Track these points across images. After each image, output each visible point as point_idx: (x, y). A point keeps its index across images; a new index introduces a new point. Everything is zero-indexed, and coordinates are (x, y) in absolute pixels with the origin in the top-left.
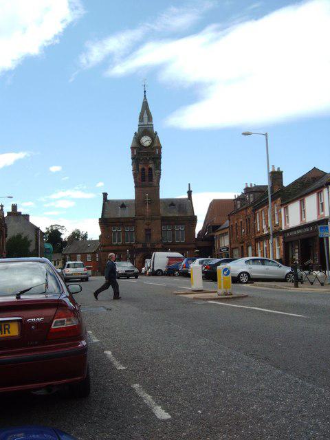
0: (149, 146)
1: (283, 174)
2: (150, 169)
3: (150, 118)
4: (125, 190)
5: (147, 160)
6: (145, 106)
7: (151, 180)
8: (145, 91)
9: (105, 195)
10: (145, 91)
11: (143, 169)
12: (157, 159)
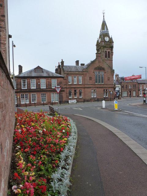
0: (107, 42)
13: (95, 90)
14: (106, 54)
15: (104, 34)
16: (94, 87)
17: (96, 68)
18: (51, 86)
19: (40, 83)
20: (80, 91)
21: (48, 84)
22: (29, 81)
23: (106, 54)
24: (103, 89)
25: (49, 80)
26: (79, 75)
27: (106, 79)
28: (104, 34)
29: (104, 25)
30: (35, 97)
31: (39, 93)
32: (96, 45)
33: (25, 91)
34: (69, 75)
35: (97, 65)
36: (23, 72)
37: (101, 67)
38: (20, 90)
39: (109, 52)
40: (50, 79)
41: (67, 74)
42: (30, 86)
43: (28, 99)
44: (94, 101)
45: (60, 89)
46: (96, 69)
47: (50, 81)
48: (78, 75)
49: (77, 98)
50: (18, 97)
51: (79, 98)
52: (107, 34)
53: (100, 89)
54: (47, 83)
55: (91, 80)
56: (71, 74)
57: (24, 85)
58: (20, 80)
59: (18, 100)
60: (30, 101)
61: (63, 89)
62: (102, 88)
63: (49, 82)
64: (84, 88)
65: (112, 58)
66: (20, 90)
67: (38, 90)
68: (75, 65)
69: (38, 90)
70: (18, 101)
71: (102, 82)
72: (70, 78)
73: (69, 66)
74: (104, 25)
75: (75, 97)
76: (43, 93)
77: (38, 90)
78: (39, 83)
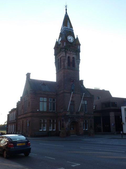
1: (84, 81)
2: (73, 58)
4: (48, 73)
5: (68, 49)
6: (67, 20)
7: (74, 66)
8: (66, 10)
9: (28, 75)
10: (66, 10)
11: (69, 57)
12: (78, 51)
29: (67, 20)
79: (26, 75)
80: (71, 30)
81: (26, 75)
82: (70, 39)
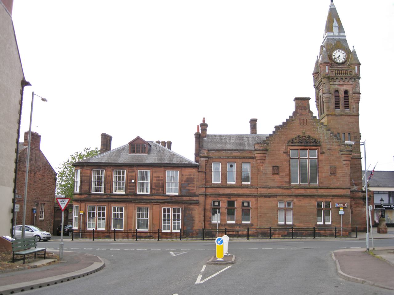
0: (343, 63)
1: (257, 122)
3: (341, 29)
9: (204, 126)
13: (289, 204)
14: (337, 98)
15: (335, 42)
16: (286, 193)
17: (293, 140)
18: (164, 189)
19: (136, 180)
20: (246, 204)
21: (155, 183)
22: (109, 173)
23: (337, 98)
24: (314, 202)
25: (159, 173)
26: (244, 160)
27: (326, 169)
28: (335, 42)
29: (333, 15)
30: (122, 216)
31: (131, 206)
32: (313, 74)
33: (98, 200)
34: (214, 160)
35: (296, 132)
36: (112, 149)
37: (309, 137)
38: (86, 196)
39: (346, 92)
40: (162, 169)
41: (209, 157)
42: (111, 186)
43: (103, 219)
44: (285, 236)
45: (67, 200)
46: (292, 143)
47: (161, 175)
48: (241, 160)
49: (236, 225)
50: (82, 213)
51: (226, 225)
52: (339, 41)
53: (305, 202)
54: (154, 181)
55: (278, 173)
56: (219, 157)
57: (282, 170)
58: (89, 172)
59: (80, 219)
60: (108, 225)
61: (195, 198)
62: (311, 196)
63: (159, 177)
64: (256, 196)
65: (358, 109)
66: (86, 196)
67: (132, 198)
68: (250, 134)
69: (130, 197)
70: (80, 222)
71: (313, 180)
72: (216, 168)
73: (220, 136)
74: (333, 15)
75: (228, 222)
76: (141, 206)
77: (130, 197)
78: (133, 181)
79: (276, 127)
80: (341, 38)
81: (276, 127)
82: (339, 56)
